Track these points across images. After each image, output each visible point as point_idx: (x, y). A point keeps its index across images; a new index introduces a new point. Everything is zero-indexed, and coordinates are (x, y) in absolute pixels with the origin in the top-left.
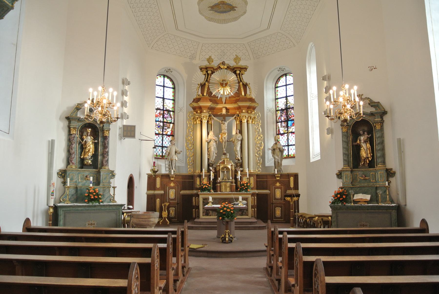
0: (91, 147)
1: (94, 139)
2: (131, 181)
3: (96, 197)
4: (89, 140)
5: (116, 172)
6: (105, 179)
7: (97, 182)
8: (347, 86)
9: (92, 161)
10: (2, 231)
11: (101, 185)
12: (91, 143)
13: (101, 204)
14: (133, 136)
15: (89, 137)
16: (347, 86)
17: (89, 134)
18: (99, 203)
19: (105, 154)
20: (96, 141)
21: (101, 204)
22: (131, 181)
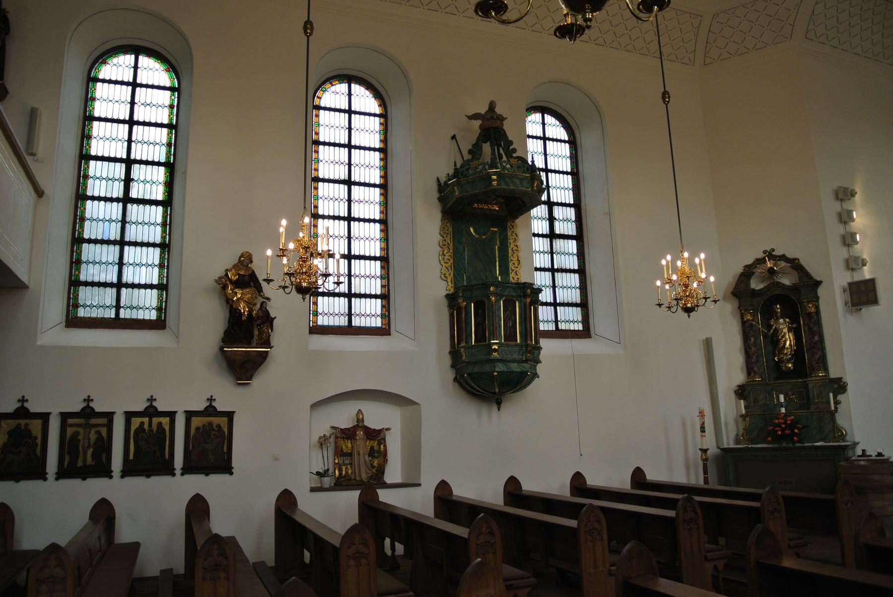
0: (789, 340)
1: (792, 322)
2: (684, 425)
3: (787, 432)
4: (783, 325)
5: (849, 379)
6: (818, 396)
7: (805, 401)
8: (686, 255)
9: (794, 364)
10: (648, 478)
11: (813, 408)
12: (785, 330)
13: (798, 445)
14: (874, 301)
15: (781, 321)
16: (686, 255)
17: (779, 315)
18: (794, 443)
19: (819, 346)
20: (795, 326)
21: (798, 445)
22: (684, 425)
